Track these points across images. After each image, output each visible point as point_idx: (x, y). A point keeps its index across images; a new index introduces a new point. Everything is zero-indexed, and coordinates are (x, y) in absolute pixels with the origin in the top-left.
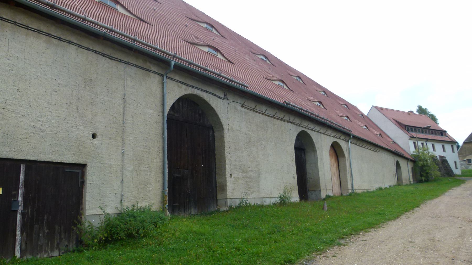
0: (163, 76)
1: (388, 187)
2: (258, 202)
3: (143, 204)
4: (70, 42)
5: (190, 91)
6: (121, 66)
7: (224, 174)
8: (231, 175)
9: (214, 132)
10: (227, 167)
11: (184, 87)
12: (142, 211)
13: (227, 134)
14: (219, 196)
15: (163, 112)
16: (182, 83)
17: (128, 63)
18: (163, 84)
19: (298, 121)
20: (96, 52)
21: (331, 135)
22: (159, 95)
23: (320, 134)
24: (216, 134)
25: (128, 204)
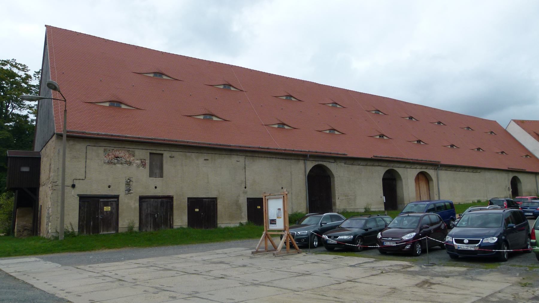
0: (305, 160)
1: (476, 201)
2: (352, 211)
3: (300, 211)
4: (273, 158)
5: (317, 163)
6: (289, 161)
7: (335, 198)
8: (338, 198)
9: (330, 178)
10: (337, 195)
11: (314, 162)
12: (299, 213)
13: (336, 179)
14: (333, 208)
15: (305, 172)
16: (313, 161)
17: (291, 159)
18: (305, 163)
19: (386, 164)
20: (281, 158)
21: (417, 168)
22: (303, 169)
23: (406, 169)
24: (332, 179)
25: (295, 211)
